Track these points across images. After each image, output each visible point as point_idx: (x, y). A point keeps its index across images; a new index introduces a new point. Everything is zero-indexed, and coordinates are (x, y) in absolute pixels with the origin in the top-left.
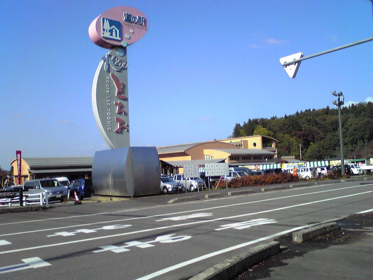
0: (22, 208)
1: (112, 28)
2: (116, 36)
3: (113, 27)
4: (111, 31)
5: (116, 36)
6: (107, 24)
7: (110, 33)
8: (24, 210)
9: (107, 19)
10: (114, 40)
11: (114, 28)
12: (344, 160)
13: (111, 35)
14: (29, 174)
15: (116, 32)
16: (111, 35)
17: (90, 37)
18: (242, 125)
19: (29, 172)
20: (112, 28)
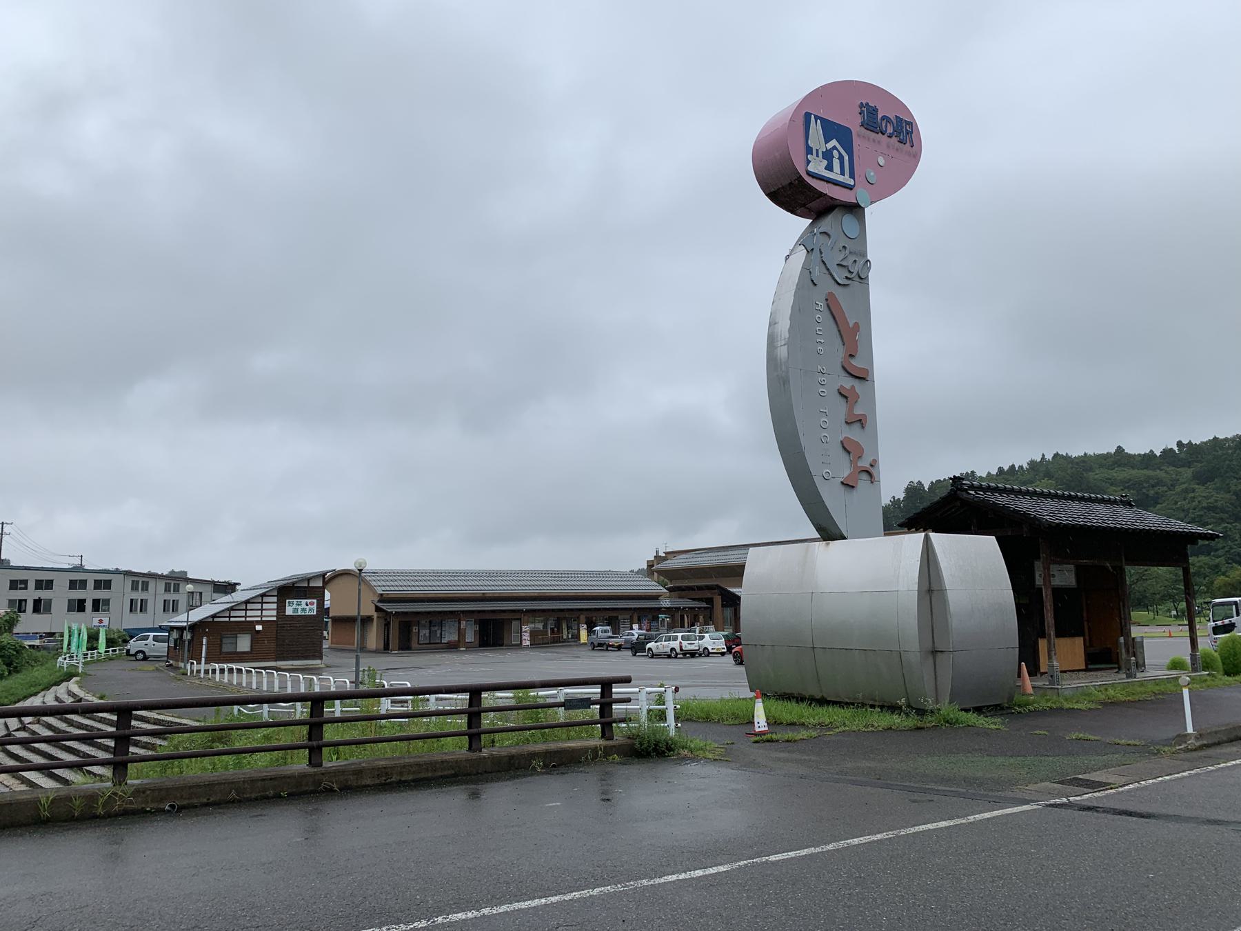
0: (315, 774)
1: (830, 146)
2: (843, 173)
3: (834, 143)
4: (828, 155)
5: (843, 173)
6: (816, 129)
7: (825, 162)
8: (934, 587)
9: (817, 118)
10: (836, 183)
11: (835, 148)
12: (757, 730)
13: (829, 168)
14: (375, 615)
15: (841, 158)
16: (829, 168)
17: (954, 623)
18: (1006, 469)
19: (378, 609)
20: (830, 146)
